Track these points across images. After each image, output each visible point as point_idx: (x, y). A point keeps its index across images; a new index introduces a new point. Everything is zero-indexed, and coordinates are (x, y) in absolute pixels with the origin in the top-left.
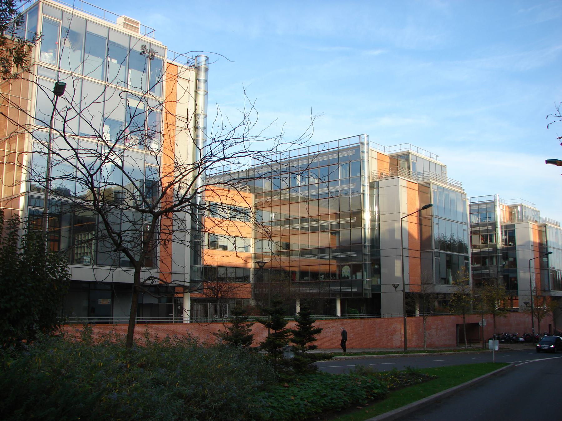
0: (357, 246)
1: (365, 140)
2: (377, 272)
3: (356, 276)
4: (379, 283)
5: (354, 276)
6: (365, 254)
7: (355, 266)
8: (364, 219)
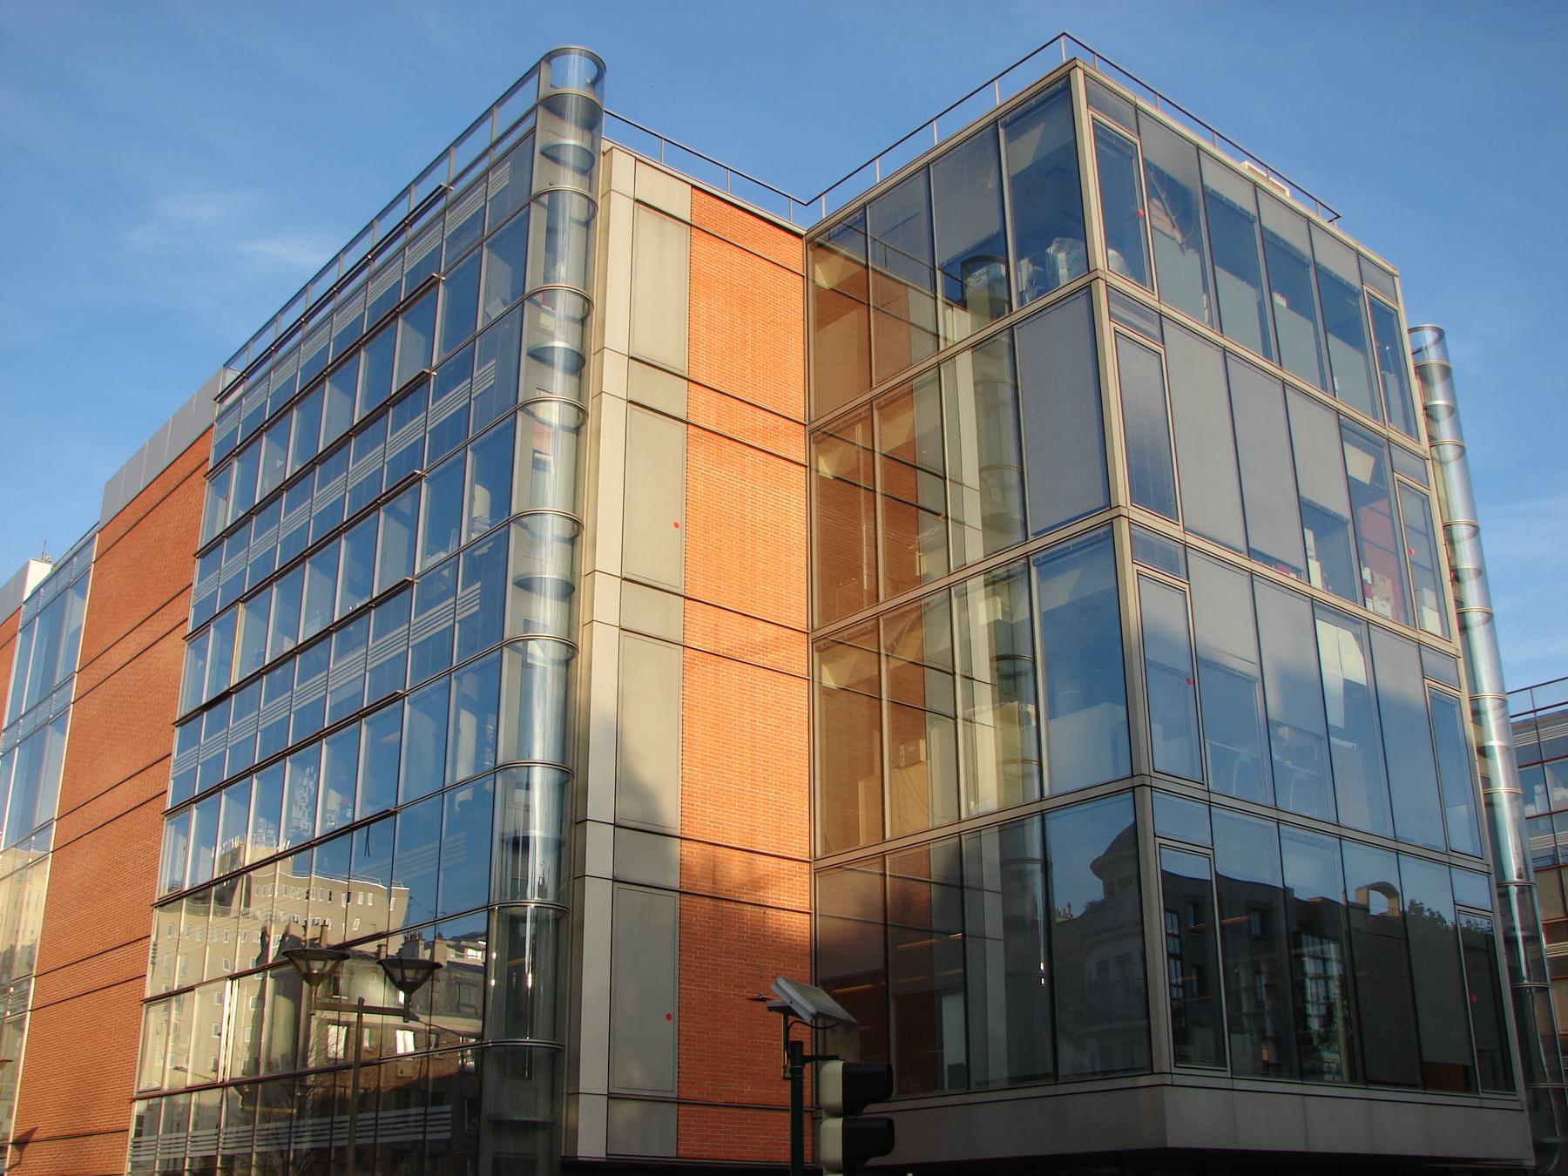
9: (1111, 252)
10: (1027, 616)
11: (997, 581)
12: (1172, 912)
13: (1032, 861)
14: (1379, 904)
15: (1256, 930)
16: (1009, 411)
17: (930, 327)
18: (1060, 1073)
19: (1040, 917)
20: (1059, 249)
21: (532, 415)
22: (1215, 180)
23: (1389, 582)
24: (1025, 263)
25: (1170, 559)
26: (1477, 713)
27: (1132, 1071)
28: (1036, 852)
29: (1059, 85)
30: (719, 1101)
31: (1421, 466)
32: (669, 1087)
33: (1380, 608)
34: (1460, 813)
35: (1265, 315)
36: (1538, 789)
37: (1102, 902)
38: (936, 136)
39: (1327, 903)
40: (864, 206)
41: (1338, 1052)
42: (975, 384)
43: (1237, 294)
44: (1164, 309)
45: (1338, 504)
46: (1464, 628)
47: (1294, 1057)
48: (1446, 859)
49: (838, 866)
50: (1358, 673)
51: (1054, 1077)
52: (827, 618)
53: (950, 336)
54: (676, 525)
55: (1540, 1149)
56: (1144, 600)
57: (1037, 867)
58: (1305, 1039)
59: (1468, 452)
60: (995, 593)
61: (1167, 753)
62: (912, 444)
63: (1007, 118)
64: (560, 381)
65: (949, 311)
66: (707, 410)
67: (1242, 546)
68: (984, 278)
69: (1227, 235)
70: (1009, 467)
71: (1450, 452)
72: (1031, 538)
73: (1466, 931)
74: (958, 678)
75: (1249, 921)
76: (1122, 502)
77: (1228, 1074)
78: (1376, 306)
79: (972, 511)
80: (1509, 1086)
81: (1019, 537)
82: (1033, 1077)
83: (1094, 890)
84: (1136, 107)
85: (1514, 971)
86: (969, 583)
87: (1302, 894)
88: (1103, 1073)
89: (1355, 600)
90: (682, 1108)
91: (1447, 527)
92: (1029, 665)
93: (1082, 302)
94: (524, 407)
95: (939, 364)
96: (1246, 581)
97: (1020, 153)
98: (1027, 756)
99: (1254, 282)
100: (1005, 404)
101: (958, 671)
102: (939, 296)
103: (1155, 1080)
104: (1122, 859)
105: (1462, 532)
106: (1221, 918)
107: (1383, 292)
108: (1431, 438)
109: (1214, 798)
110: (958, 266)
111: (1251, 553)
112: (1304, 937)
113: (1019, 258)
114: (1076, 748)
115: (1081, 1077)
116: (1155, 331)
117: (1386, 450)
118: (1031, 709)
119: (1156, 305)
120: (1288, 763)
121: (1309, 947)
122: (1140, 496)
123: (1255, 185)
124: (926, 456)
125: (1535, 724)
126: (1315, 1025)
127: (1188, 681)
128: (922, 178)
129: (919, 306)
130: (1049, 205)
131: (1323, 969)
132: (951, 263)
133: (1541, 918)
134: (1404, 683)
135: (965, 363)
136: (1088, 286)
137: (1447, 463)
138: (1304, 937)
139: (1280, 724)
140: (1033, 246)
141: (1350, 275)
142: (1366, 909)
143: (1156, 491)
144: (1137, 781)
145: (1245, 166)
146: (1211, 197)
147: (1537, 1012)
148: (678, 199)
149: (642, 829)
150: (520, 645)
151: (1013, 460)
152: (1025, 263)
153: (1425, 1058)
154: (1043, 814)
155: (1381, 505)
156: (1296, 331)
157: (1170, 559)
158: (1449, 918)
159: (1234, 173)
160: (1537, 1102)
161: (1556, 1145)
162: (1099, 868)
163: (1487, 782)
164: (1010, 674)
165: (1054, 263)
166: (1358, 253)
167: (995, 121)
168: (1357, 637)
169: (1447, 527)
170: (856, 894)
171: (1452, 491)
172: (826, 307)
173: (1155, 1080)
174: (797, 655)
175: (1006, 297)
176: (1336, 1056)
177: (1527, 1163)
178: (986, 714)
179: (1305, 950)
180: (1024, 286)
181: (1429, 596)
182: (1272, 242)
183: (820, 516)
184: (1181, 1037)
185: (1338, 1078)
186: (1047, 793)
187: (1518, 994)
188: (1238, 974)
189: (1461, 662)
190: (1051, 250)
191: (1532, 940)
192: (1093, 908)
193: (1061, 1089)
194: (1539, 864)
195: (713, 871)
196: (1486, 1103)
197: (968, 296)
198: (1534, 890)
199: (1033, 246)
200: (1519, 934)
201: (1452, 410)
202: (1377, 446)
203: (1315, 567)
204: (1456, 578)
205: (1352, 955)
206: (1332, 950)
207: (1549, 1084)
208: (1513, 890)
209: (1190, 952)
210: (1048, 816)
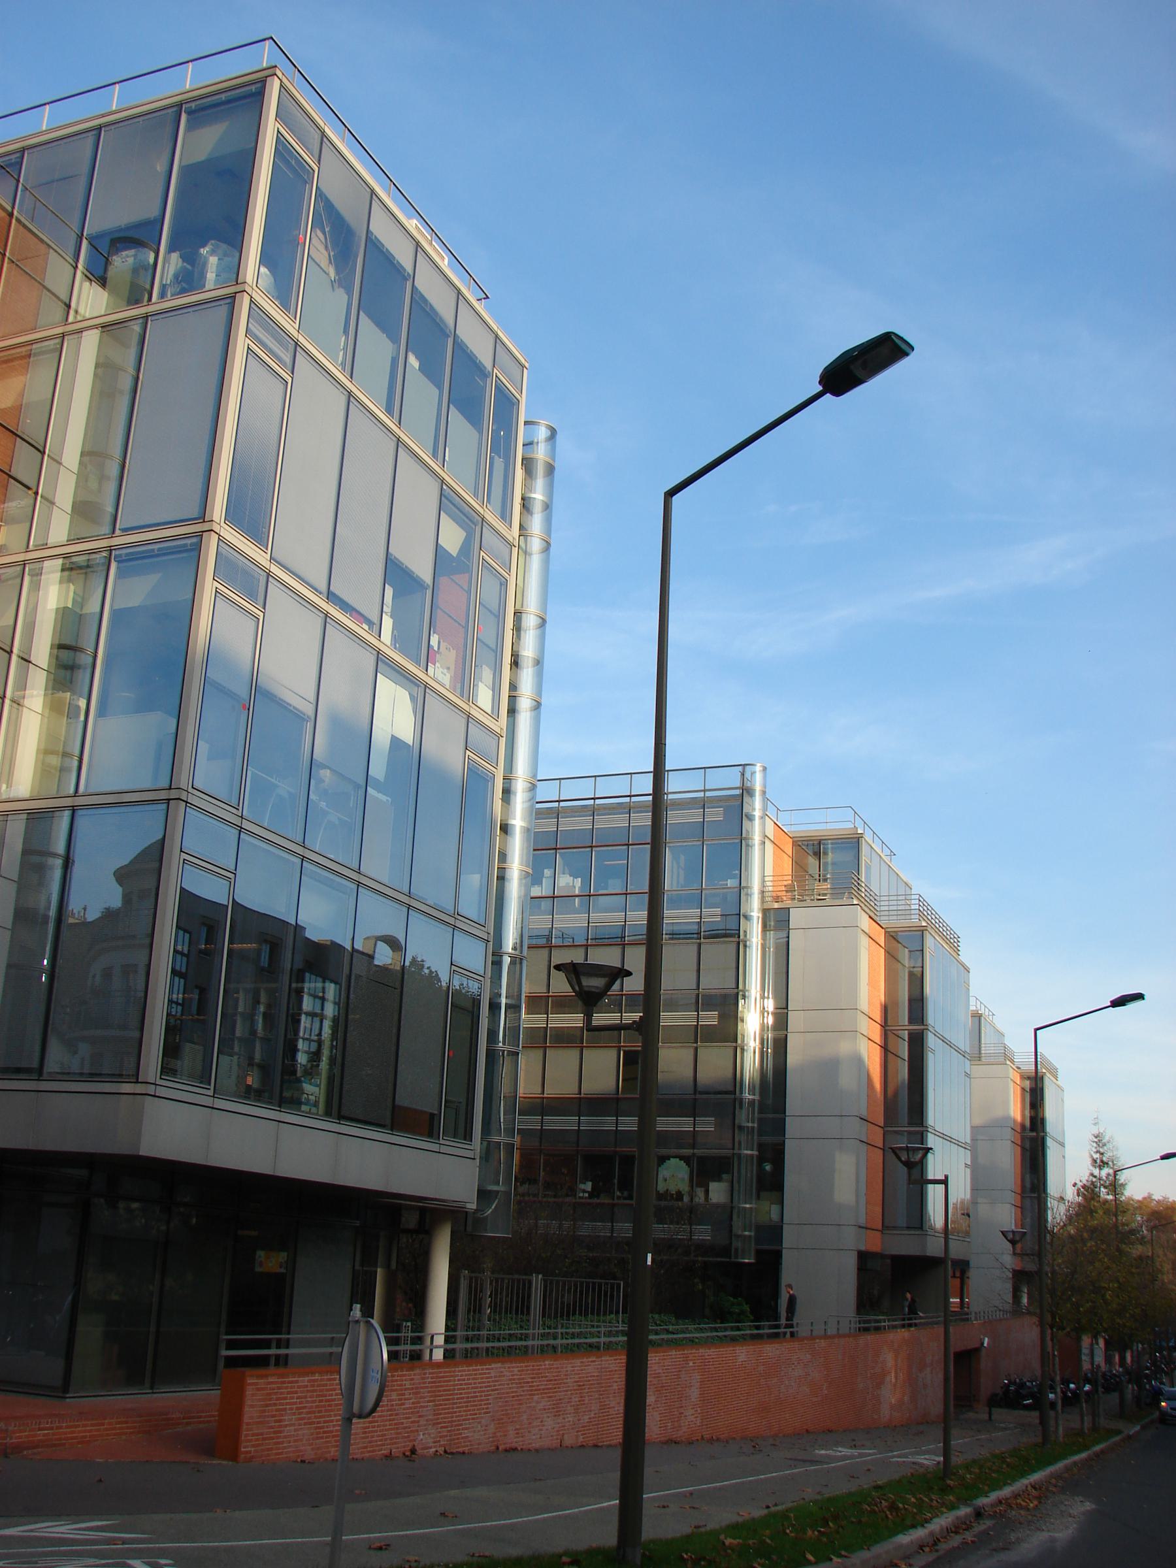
2: (772, 1183)
3: (707, 1192)
4: (775, 1216)
5: (700, 1192)
6: (741, 1128)
7: (702, 1160)
9: (263, 270)
10: (98, 609)
11: (74, 568)
12: (185, 931)
13: (55, 855)
14: (384, 956)
15: (264, 961)
16: (123, 403)
17: (64, 296)
18: (45, 1070)
19: (52, 913)
20: (213, 252)
22: (380, 228)
23: (453, 653)
24: (175, 256)
25: (250, 584)
26: (507, 792)
27: (118, 1077)
28: (60, 848)
29: (253, 88)
31: (508, 551)
33: (440, 675)
34: (473, 881)
35: (396, 370)
36: (548, 872)
37: (119, 909)
38: (115, 101)
39: (335, 947)
40: (23, 151)
41: (319, 1086)
42: (97, 366)
43: (375, 345)
44: (301, 339)
45: (423, 569)
46: (512, 711)
47: (276, 1085)
48: (452, 921)
50: (407, 734)
51: (38, 1072)
53: (81, 310)
55: (484, 1195)
56: (217, 620)
57: (59, 862)
58: (290, 1070)
59: (552, 549)
60: (70, 580)
61: (208, 772)
62: (18, 409)
63: (193, 105)
65: (87, 284)
67: (324, 588)
68: (131, 260)
69: (378, 284)
70: (110, 459)
71: (536, 544)
72: (118, 532)
73: (457, 993)
74: (14, 658)
75: (259, 951)
76: (216, 517)
77: (211, 1093)
78: (501, 391)
79: (65, 492)
80: (468, 1136)
81: (106, 529)
82: (18, 1070)
83: (114, 897)
84: (323, 134)
85: (492, 1035)
86: (47, 564)
87: (313, 935)
88: (91, 1075)
89: (418, 663)
91: (518, 614)
92: (90, 660)
93: (223, 310)
95: (63, 335)
96: (319, 621)
97: (198, 144)
98: (69, 750)
99: (394, 338)
100: (121, 393)
101: (15, 650)
102: (80, 266)
103: (139, 1088)
104: (145, 871)
105: (530, 621)
106: (231, 942)
107: (511, 380)
108: (521, 527)
109: (246, 825)
110: (107, 240)
111: (331, 596)
112: (307, 975)
113: (171, 249)
114: (120, 750)
115: (66, 1075)
116: (288, 359)
117: (478, 529)
118: (82, 703)
119: (295, 333)
120: (323, 804)
121: (311, 984)
122: (233, 515)
123: (418, 245)
124: (29, 426)
125: (557, 814)
126: (302, 1058)
127: (244, 706)
128: (90, 139)
129: (57, 271)
130: (212, 208)
131: (320, 1006)
132: (100, 236)
133: (526, 989)
134: (447, 752)
135: (91, 339)
136: (233, 297)
137: (530, 554)
138: (307, 975)
139: (323, 766)
140: (188, 241)
141: (484, 356)
142: (371, 957)
143: (251, 514)
144: (174, 794)
145: (412, 224)
146: (372, 243)
147: (506, 1070)
151: (117, 452)
152: (175, 256)
153: (398, 1102)
154: (74, 810)
155: (462, 579)
156: (422, 395)
157: (250, 584)
158: (444, 978)
159: (399, 228)
160: (487, 1155)
161: (497, 1192)
162: (121, 876)
163: (503, 857)
164: (69, 663)
165: (205, 264)
166: (497, 336)
167: (180, 105)
168: (413, 699)
169: (518, 614)
171: (530, 585)
173: (139, 1088)
175: (148, 287)
176: (317, 1089)
177: (469, 1206)
178: (36, 699)
179: (306, 985)
180: (168, 279)
181: (487, 674)
182: (420, 303)
184: (171, 1050)
185: (314, 1110)
186: (82, 789)
187: (491, 1055)
188: (237, 999)
189: (503, 741)
190: (204, 251)
191: (514, 1008)
192: (109, 915)
193: (44, 1085)
194: (534, 942)
196: (444, 1149)
197: (110, 274)
198: (525, 963)
199: (188, 241)
200: (503, 1001)
201: (547, 507)
202: (471, 522)
203: (388, 623)
204: (515, 663)
205: (348, 997)
206: (331, 990)
207: (502, 1138)
208: (507, 960)
209: (195, 971)
210: (80, 813)
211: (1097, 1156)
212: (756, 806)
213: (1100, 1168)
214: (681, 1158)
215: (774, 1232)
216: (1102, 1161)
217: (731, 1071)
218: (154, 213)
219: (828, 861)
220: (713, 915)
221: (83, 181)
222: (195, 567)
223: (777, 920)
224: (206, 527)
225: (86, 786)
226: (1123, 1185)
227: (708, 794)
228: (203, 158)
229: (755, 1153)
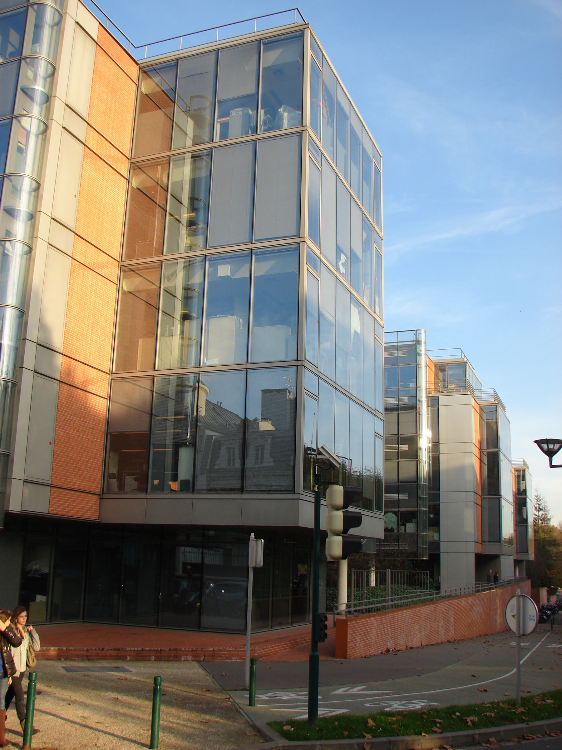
0: (411, 485)
1: (423, 338)
2: (435, 523)
5: (402, 528)
6: (420, 498)
7: (403, 513)
8: (420, 449)
20: (284, 111)
21: (19, 122)
30: (66, 487)
32: (46, 477)
40: (178, 60)
49: (122, 379)
52: (130, 256)
54: (75, 196)
63: (267, 40)
64: (36, 110)
66: (94, 142)
72: (254, 242)
90: (53, 489)
93: (296, 139)
94: (16, 117)
97: (270, 58)
103: (295, 496)
109: (321, 375)
113: (262, 109)
128: (213, 56)
136: (301, 133)
144: (299, 363)
148: (93, 27)
149: (46, 347)
150: (3, 243)
167: (260, 40)
170: (138, 393)
172: (147, 103)
174: (113, 272)
183: (131, 206)
186: (249, 361)
195: (69, 372)
211: (537, 505)
212: (422, 349)
213: (538, 511)
214: (393, 512)
215: (436, 545)
216: (539, 508)
217: (415, 472)
218: (253, 91)
219: (453, 375)
220: (404, 400)
221: (212, 76)
222: (298, 256)
223: (434, 403)
224: (301, 240)
225: (251, 360)
226: (549, 519)
227: (399, 344)
228: (270, 65)
229: (427, 509)
